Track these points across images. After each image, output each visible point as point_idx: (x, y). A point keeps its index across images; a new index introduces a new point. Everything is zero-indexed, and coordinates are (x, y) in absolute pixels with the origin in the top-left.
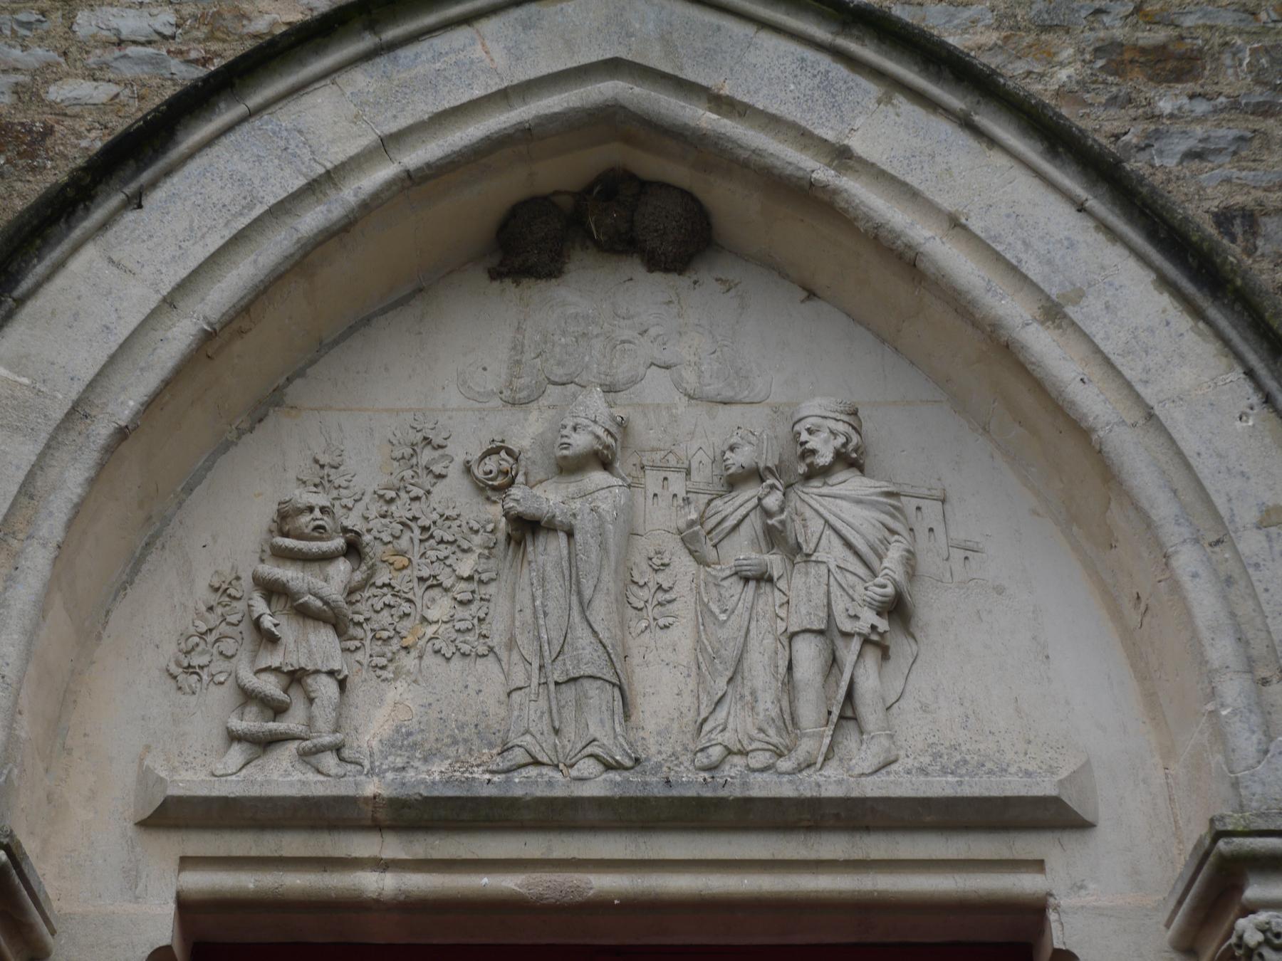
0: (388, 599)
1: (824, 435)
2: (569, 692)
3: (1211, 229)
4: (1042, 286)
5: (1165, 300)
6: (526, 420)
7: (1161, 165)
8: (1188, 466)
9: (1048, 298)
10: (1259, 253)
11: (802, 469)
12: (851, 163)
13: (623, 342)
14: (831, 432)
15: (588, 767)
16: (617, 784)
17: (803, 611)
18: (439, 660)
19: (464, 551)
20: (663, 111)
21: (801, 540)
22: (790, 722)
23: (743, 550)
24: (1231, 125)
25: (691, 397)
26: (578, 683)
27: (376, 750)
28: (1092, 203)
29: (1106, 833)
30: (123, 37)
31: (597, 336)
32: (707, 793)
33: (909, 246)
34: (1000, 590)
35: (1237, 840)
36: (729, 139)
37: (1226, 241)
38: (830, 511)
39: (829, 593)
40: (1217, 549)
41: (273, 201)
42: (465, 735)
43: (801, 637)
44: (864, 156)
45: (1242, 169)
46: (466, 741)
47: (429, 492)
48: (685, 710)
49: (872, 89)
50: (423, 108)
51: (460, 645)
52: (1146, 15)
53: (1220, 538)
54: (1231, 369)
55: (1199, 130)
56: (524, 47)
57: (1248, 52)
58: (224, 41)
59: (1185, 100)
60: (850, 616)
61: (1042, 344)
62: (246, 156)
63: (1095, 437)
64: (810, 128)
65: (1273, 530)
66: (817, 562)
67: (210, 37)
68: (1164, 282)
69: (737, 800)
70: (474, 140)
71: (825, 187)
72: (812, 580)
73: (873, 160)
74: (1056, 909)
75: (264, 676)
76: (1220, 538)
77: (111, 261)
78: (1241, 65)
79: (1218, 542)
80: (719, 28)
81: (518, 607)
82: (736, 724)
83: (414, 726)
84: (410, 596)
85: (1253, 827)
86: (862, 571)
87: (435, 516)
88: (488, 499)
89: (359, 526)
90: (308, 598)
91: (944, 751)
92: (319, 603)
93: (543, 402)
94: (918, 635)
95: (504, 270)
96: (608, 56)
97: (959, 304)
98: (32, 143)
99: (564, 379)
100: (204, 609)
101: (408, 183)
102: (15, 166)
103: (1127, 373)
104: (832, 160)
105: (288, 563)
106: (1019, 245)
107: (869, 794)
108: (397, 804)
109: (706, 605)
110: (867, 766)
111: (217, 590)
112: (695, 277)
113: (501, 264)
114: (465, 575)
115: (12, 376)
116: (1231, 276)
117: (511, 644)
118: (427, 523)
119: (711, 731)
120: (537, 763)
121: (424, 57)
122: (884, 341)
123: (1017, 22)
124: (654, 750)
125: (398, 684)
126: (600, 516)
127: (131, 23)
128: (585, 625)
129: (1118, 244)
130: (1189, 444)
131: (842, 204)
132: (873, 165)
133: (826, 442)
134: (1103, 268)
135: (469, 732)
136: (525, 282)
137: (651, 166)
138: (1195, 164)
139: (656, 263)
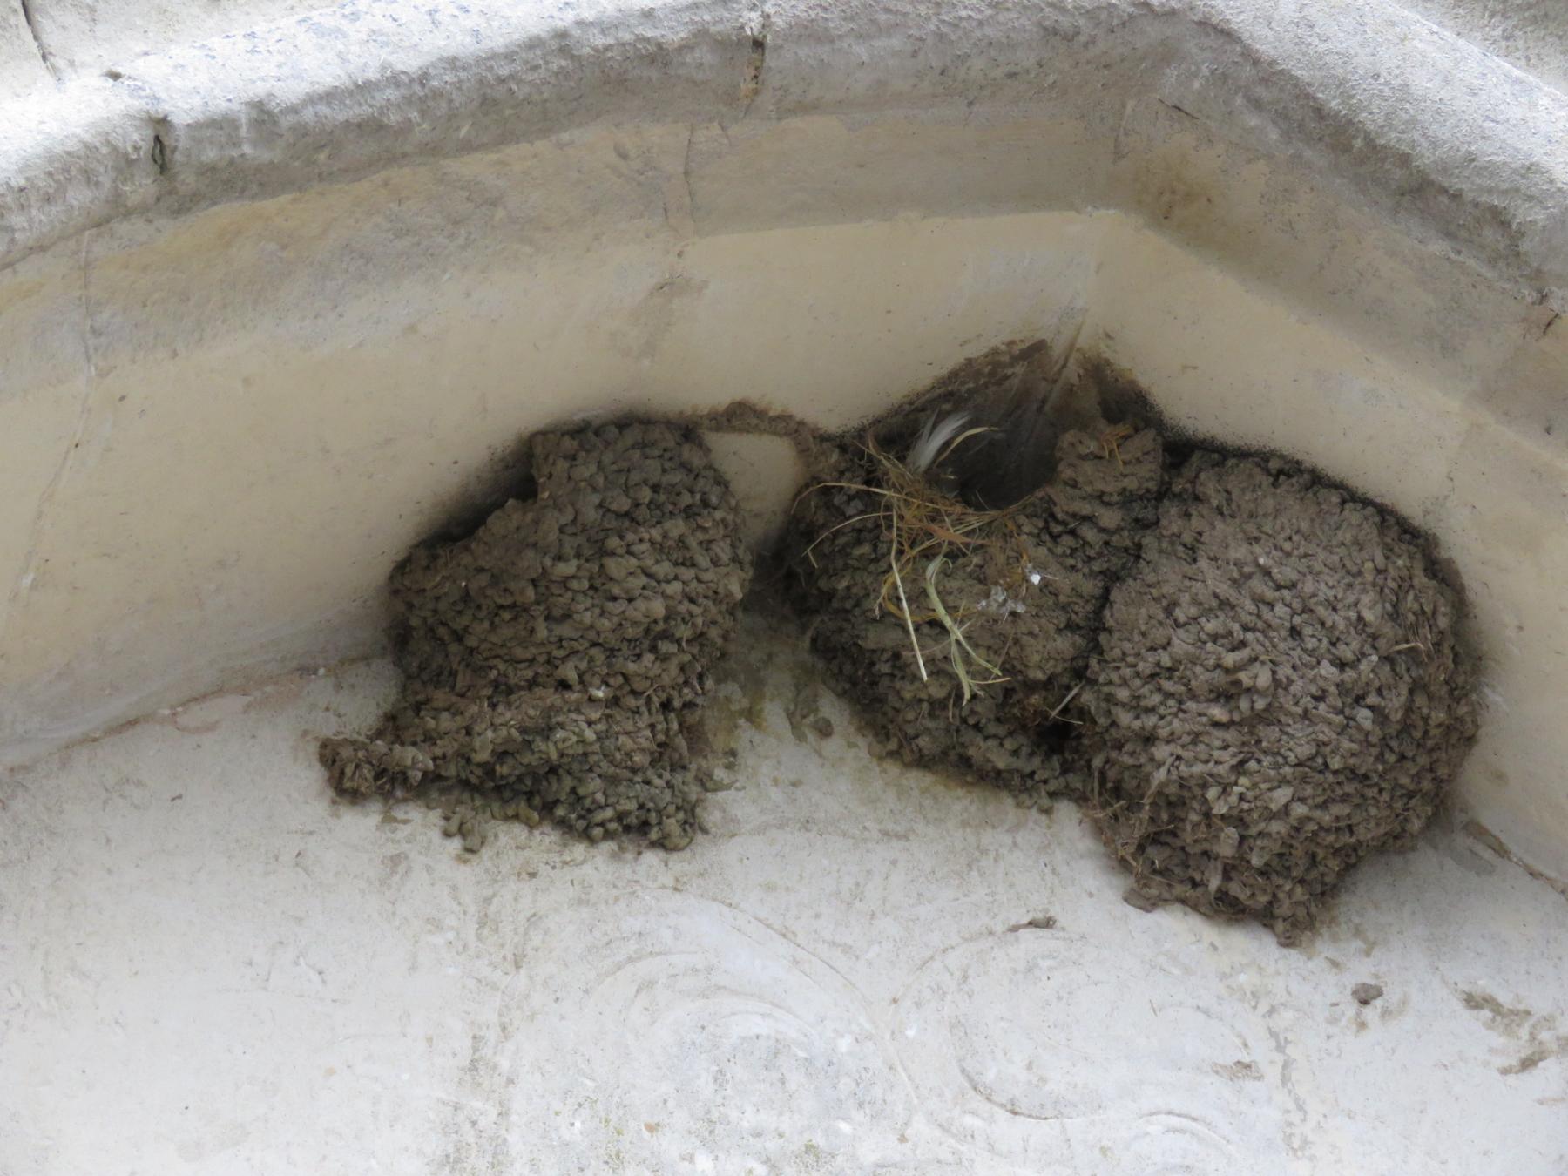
20: (1422, 83)
70: (498, 38)
95: (416, 758)
101: (143, 186)
112: (1362, 971)
113: (393, 726)
136: (515, 843)
137: (1234, 354)
139: (1178, 858)
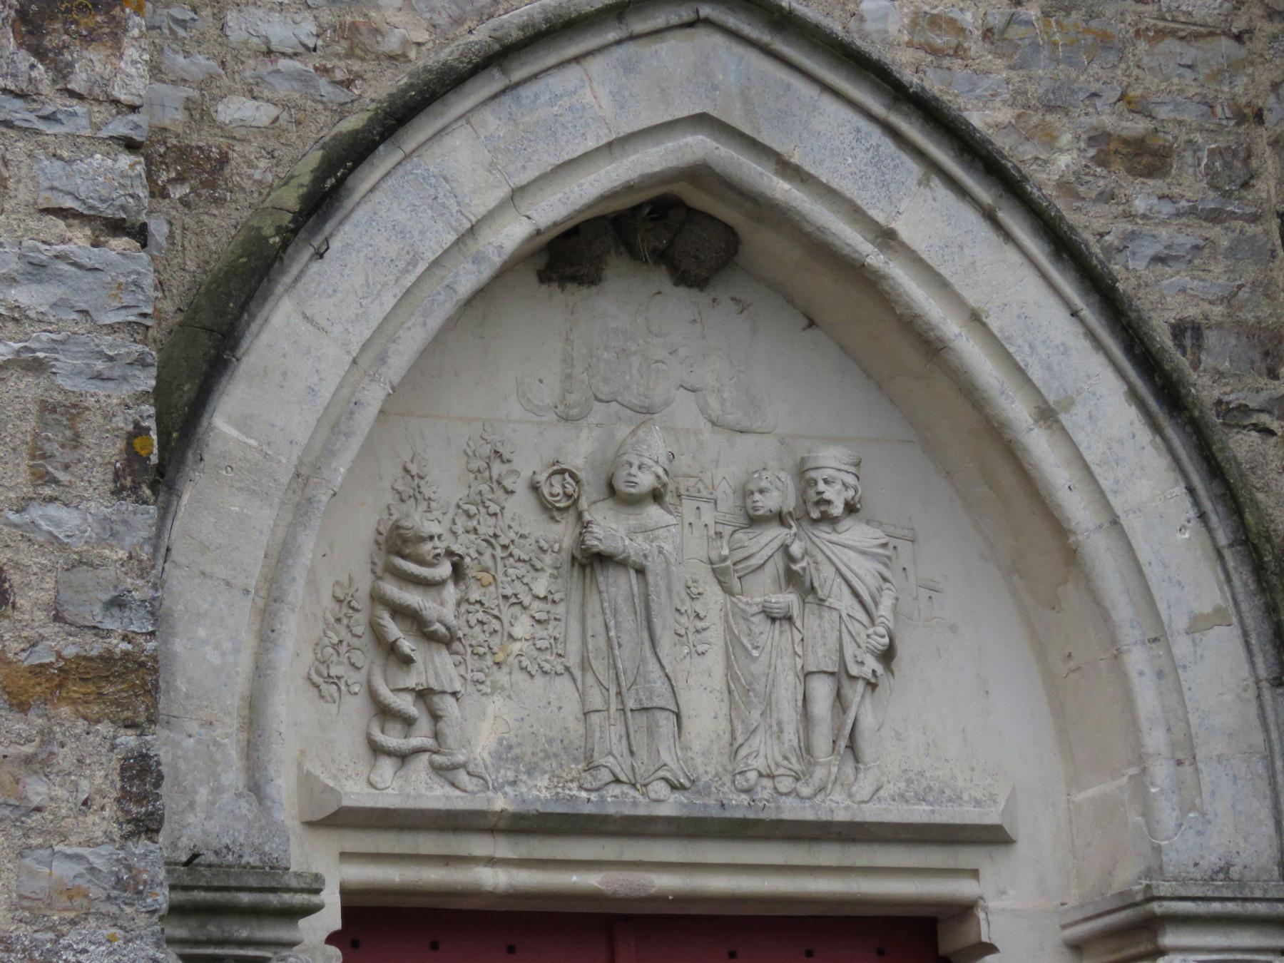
0: (480, 616)
1: (838, 486)
2: (642, 719)
3: (1169, 342)
4: (1043, 390)
5: (1132, 412)
6: (578, 437)
7: (1130, 273)
8: (1140, 572)
9: (1046, 402)
10: (1202, 368)
11: (815, 514)
12: (892, 243)
13: (657, 362)
14: (844, 484)
15: (660, 789)
16: (684, 806)
17: (820, 654)
18: (526, 676)
19: (537, 570)
21: (816, 585)
22: (807, 749)
23: (765, 590)
24: (1189, 230)
25: (714, 424)
26: (650, 713)
27: (488, 763)
28: (1086, 313)
29: (1023, 846)
30: (274, 48)
31: (635, 353)
32: (751, 815)
33: (940, 340)
34: (954, 629)
35: (1166, 904)
36: (798, 213)
37: (1179, 354)
38: (841, 560)
39: (840, 638)
40: (1153, 645)
41: (432, 258)
42: (554, 750)
43: (816, 677)
44: (907, 242)
45: (1193, 278)
46: (556, 755)
47: (503, 508)
48: (721, 733)
49: (913, 168)
50: (547, 158)
51: (543, 664)
52: (1129, 103)
53: (1158, 638)
54: (1177, 484)
55: (1164, 233)
56: (627, 94)
57: (1206, 153)
58: (363, 59)
59: (1156, 201)
60: (857, 662)
61: (1040, 446)
62: (404, 205)
63: (1072, 539)
64: (865, 207)
65: (1197, 635)
66: (829, 608)
67: (350, 55)
68: (1133, 394)
69: (772, 821)
71: (875, 272)
72: (826, 625)
73: (915, 248)
74: (985, 910)
75: (403, 695)
76: (1158, 638)
77: (305, 317)
78: (1199, 165)
79: (1155, 640)
80: (788, 87)
81: (590, 633)
82: (762, 751)
83: (514, 741)
84: (496, 612)
85: (1177, 894)
86: (863, 617)
87: (512, 535)
88: (553, 518)
89: (461, 551)
90: (437, 626)
91: (914, 777)
92: (443, 630)
93: (592, 419)
94: (896, 673)
96: (698, 111)
97: (969, 392)
98: (212, 172)
99: (609, 397)
100: (332, 620)
102: (199, 196)
103: (1103, 483)
104: (876, 237)
105: (411, 587)
106: (1027, 349)
107: (869, 819)
108: (517, 817)
109: (738, 638)
110: (865, 795)
111: (340, 601)
114: (542, 595)
115: (243, 438)
116: (1191, 407)
117: (585, 664)
118: (506, 542)
119: (747, 757)
120: (618, 781)
121: (542, 99)
122: (869, 376)
123: (1028, 99)
124: (706, 769)
125: (495, 698)
126: (666, 557)
127: (280, 31)
128: (654, 660)
129: (1101, 353)
130: (1144, 555)
131: (887, 288)
132: (914, 252)
133: (839, 493)
134: (1088, 377)
135: (556, 747)
136: (569, 286)
138: (1159, 267)
